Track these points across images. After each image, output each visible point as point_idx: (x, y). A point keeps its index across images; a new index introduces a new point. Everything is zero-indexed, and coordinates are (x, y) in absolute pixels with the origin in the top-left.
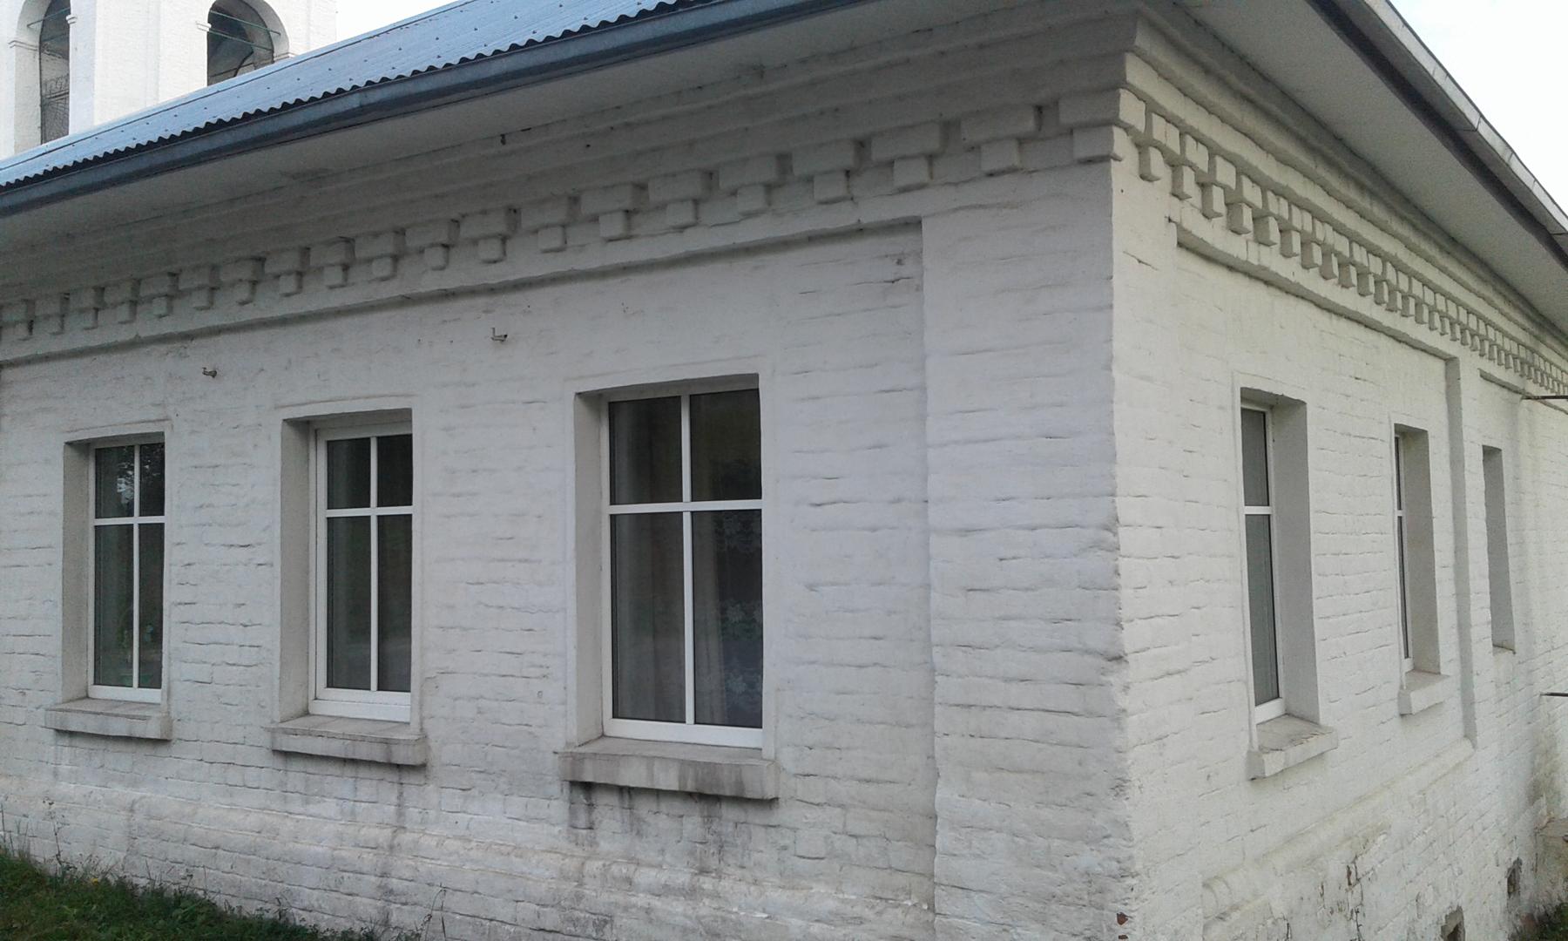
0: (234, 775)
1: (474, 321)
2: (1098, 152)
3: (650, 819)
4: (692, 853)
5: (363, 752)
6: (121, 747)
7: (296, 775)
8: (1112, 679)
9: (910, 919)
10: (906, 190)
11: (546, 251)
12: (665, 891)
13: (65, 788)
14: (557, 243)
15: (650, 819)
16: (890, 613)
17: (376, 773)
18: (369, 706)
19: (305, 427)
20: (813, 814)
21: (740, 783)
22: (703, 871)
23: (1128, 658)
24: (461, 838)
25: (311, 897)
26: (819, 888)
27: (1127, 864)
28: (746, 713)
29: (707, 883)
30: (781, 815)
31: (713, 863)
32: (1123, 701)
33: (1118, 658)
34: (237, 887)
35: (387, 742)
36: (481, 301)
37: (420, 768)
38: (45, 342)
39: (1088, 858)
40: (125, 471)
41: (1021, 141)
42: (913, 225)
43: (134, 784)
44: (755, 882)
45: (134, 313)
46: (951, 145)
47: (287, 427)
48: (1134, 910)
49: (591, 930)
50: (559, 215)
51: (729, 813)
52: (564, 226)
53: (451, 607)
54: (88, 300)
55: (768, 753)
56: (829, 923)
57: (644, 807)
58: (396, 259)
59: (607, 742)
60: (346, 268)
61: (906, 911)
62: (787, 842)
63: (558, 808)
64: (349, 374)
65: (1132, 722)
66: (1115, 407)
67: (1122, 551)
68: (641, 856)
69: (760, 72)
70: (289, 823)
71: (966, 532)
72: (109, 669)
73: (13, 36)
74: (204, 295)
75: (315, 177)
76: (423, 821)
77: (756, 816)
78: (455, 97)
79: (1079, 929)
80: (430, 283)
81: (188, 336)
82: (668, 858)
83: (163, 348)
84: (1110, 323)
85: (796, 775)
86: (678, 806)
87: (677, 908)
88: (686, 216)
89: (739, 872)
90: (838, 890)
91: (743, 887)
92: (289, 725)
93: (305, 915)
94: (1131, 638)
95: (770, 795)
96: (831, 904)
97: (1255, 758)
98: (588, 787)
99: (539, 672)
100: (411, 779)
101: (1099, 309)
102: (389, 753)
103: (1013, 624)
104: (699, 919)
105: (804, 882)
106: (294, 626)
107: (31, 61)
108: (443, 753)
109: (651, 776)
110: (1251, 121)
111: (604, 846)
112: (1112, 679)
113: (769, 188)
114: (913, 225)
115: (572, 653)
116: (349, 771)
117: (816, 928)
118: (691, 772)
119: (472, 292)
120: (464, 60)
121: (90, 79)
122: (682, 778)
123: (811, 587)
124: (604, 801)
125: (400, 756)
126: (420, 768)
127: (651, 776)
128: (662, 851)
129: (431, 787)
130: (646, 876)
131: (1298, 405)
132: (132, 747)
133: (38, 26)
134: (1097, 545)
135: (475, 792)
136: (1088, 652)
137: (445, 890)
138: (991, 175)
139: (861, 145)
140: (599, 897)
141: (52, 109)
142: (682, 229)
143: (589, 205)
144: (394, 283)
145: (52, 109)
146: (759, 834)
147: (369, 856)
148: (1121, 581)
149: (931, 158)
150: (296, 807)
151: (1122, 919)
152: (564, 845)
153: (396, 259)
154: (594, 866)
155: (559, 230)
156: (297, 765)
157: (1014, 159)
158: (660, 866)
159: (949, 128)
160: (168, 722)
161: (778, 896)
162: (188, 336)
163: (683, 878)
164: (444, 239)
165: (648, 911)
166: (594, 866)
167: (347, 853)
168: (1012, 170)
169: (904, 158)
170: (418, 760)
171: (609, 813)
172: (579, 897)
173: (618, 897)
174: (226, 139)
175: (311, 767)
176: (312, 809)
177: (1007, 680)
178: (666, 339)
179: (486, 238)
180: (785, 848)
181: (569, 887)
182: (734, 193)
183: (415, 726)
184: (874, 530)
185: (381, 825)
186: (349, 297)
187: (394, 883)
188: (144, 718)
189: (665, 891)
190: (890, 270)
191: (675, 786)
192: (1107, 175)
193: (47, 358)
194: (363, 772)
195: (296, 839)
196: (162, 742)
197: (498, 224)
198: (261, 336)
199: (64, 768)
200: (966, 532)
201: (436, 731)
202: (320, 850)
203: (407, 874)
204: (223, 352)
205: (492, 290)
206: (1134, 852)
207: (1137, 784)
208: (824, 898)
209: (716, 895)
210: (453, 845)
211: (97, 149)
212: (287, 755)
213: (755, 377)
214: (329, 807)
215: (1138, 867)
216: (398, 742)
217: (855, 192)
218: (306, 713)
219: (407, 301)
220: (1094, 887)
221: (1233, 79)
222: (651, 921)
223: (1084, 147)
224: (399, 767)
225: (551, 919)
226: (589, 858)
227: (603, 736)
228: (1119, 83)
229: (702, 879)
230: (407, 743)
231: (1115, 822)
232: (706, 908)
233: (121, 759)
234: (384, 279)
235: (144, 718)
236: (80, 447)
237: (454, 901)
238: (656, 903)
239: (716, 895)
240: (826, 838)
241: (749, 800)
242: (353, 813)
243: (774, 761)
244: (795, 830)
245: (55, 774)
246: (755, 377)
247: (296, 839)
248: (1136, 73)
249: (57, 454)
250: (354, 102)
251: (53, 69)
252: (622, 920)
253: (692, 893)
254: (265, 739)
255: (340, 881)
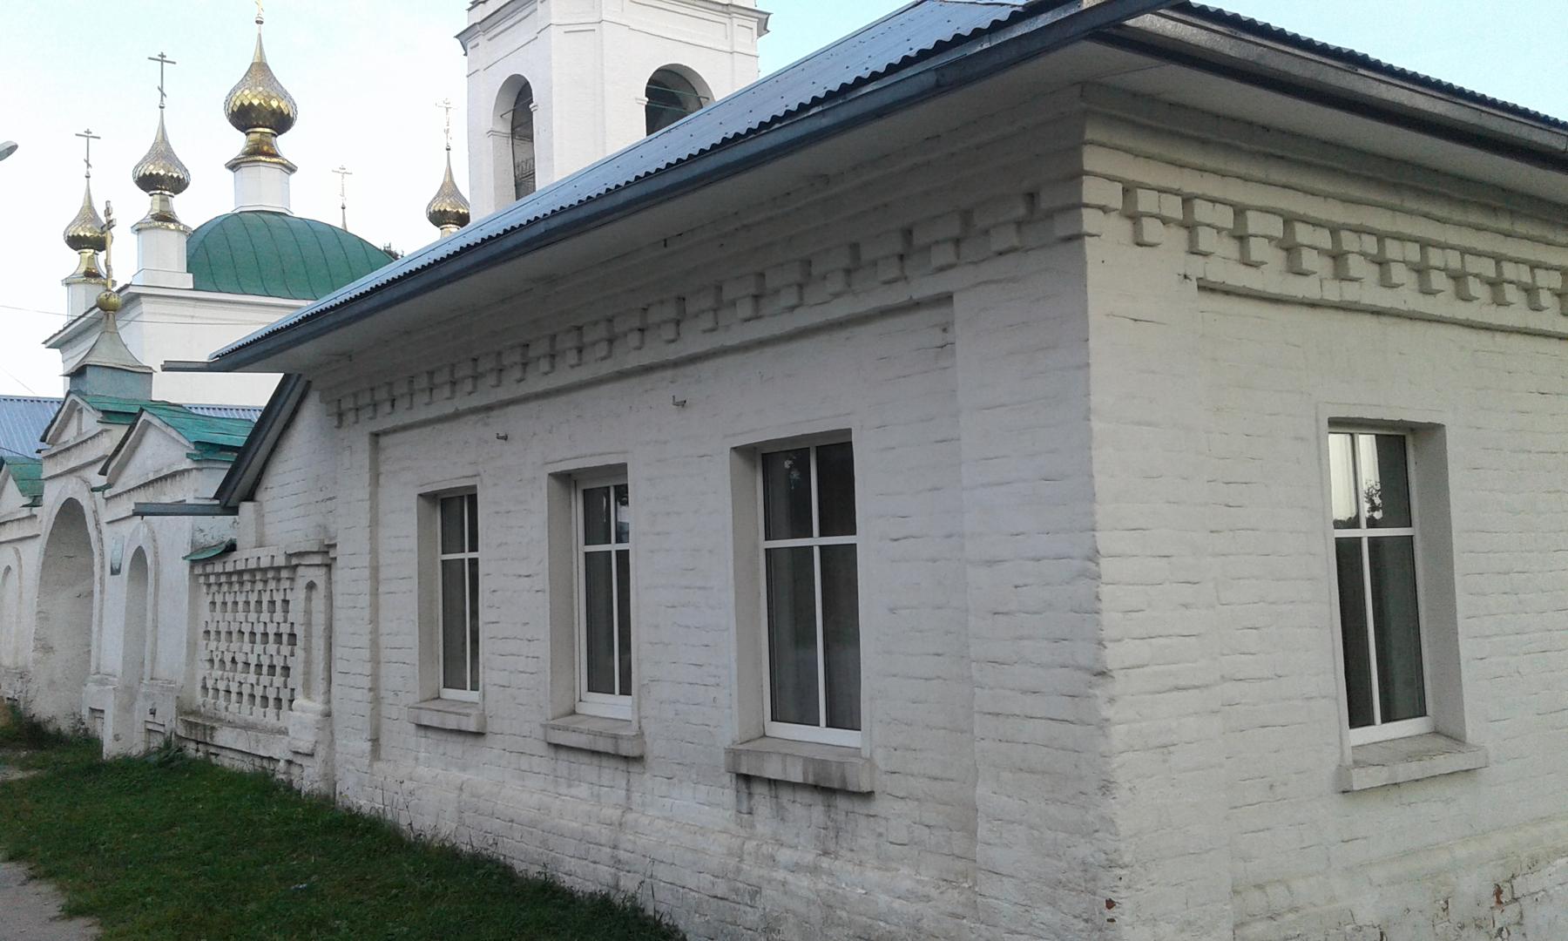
0: (524, 762)
1: (663, 389)
2: (1069, 232)
3: (789, 806)
4: (817, 837)
5: (601, 745)
6: (455, 738)
7: (564, 763)
8: (1097, 692)
9: (962, 899)
10: (942, 269)
11: (705, 331)
12: (795, 868)
13: (422, 771)
14: (710, 325)
15: (789, 806)
16: (947, 633)
17: (612, 763)
18: (609, 707)
19: (566, 479)
20: (899, 806)
21: (844, 779)
22: (826, 853)
23: (1114, 674)
24: (666, 819)
25: (571, 864)
26: (904, 871)
27: (1115, 856)
28: (843, 714)
29: (825, 862)
30: (880, 806)
31: (832, 846)
32: (1108, 712)
33: (1102, 674)
34: (524, 855)
35: (615, 737)
36: (669, 373)
37: (639, 759)
38: (402, 417)
39: (1084, 850)
40: (454, 511)
41: (1019, 224)
42: (946, 299)
43: (464, 769)
44: (861, 863)
45: (453, 392)
46: (967, 234)
47: (422, 501)
48: (1120, 896)
49: (747, 899)
50: (708, 302)
51: (842, 803)
52: (715, 310)
53: (657, 627)
54: (423, 382)
55: (865, 753)
56: (907, 899)
57: (786, 796)
58: (611, 341)
59: (764, 741)
60: (580, 351)
61: (961, 894)
62: (881, 830)
63: (728, 796)
64: (583, 434)
65: (1118, 733)
66: (1094, 453)
67: (1104, 579)
68: (784, 838)
69: (826, 179)
70: (558, 802)
71: (991, 563)
72: (453, 679)
73: (490, 126)
74: (604, 345)
75: (550, 280)
76: (643, 804)
77: (859, 807)
78: (606, 219)
79: (1077, 912)
80: (633, 361)
81: (489, 408)
82: (802, 840)
83: (474, 418)
84: (1088, 380)
85: (887, 772)
86: (805, 797)
87: (803, 883)
88: (893, 272)
89: (849, 855)
90: (918, 873)
91: (849, 867)
92: (556, 722)
93: (567, 878)
94: (1113, 656)
95: (865, 788)
96: (908, 884)
97: (1342, 772)
98: (747, 779)
99: (712, 681)
100: (635, 768)
101: (1079, 368)
102: (616, 746)
103: (1026, 642)
104: (818, 893)
105: (894, 865)
106: (560, 640)
107: (505, 145)
108: (656, 748)
109: (784, 769)
110: (1278, 174)
111: (760, 829)
112: (1097, 692)
113: (848, 272)
114: (946, 299)
115: (734, 666)
116: (595, 760)
117: (897, 904)
118: (811, 769)
119: (663, 366)
120: (647, 174)
121: (550, 159)
122: (805, 773)
123: (892, 610)
124: (760, 790)
125: (626, 749)
126: (639, 759)
127: (784, 769)
128: (797, 835)
129: (647, 776)
130: (785, 855)
131: (1440, 427)
132: (461, 739)
133: (510, 116)
134: (1083, 574)
135: (675, 780)
136: (1079, 668)
137: (653, 861)
138: (1000, 254)
139: (908, 233)
140: (754, 871)
141: (523, 182)
142: (792, 308)
143: (729, 293)
144: (608, 362)
145: (523, 182)
146: (863, 822)
147: (605, 831)
148: (1102, 606)
149: (957, 242)
150: (563, 790)
151: (1110, 904)
152: (732, 827)
153: (611, 341)
154: (750, 846)
155: (711, 314)
156: (563, 755)
157: (1015, 241)
158: (795, 847)
159: (966, 216)
160: (483, 717)
161: (872, 875)
162: (489, 408)
163: (809, 858)
164: (638, 324)
165: (784, 884)
166: (750, 846)
167: (593, 829)
168: (1013, 250)
169: (937, 243)
170: (636, 752)
171: (762, 800)
172: (739, 870)
173: (764, 872)
174: (471, 259)
175: (572, 757)
176: (574, 791)
177: (1024, 692)
178: (788, 405)
179: (665, 322)
180: (880, 835)
181: (733, 862)
182: (825, 278)
183: (635, 725)
184: (935, 561)
185: (616, 806)
186: (584, 374)
187: (622, 855)
188: (467, 715)
189: (795, 868)
190: (939, 338)
191: (800, 780)
192: (1082, 247)
193: (405, 428)
194: (605, 762)
195: (561, 816)
196: (479, 734)
197: (670, 312)
198: (533, 406)
199: (422, 755)
200: (991, 563)
201: (649, 728)
202: (575, 824)
203: (630, 847)
204: (513, 420)
205: (676, 364)
206: (1122, 846)
207: (1128, 785)
208: (905, 879)
209: (831, 874)
210: (660, 823)
211: (417, 264)
212: (557, 747)
213: (849, 431)
214: (582, 790)
215: (1127, 859)
216: (622, 737)
217: (907, 273)
218: (573, 713)
219: (622, 375)
220: (1089, 876)
221: (1244, 145)
222: (786, 893)
223: (1061, 228)
224: (626, 758)
225: (721, 889)
226: (749, 838)
227: (764, 736)
228: (1077, 175)
229: (823, 859)
230: (629, 738)
231: (1103, 818)
232: (822, 884)
233: (455, 747)
234: (603, 359)
235: (467, 715)
236: (429, 498)
237: (662, 872)
238: (790, 878)
239: (831, 874)
240: (909, 827)
241: (854, 794)
242: (598, 796)
243: (870, 760)
244: (886, 819)
245: (417, 759)
246: (849, 431)
247: (561, 816)
248: (1093, 159)
249: (413, 503)
250: (541, 228)
251: (522, 147)
252: (768, 891)
253: (814, 870)
254: (539, 732)
255: (588, 851)
